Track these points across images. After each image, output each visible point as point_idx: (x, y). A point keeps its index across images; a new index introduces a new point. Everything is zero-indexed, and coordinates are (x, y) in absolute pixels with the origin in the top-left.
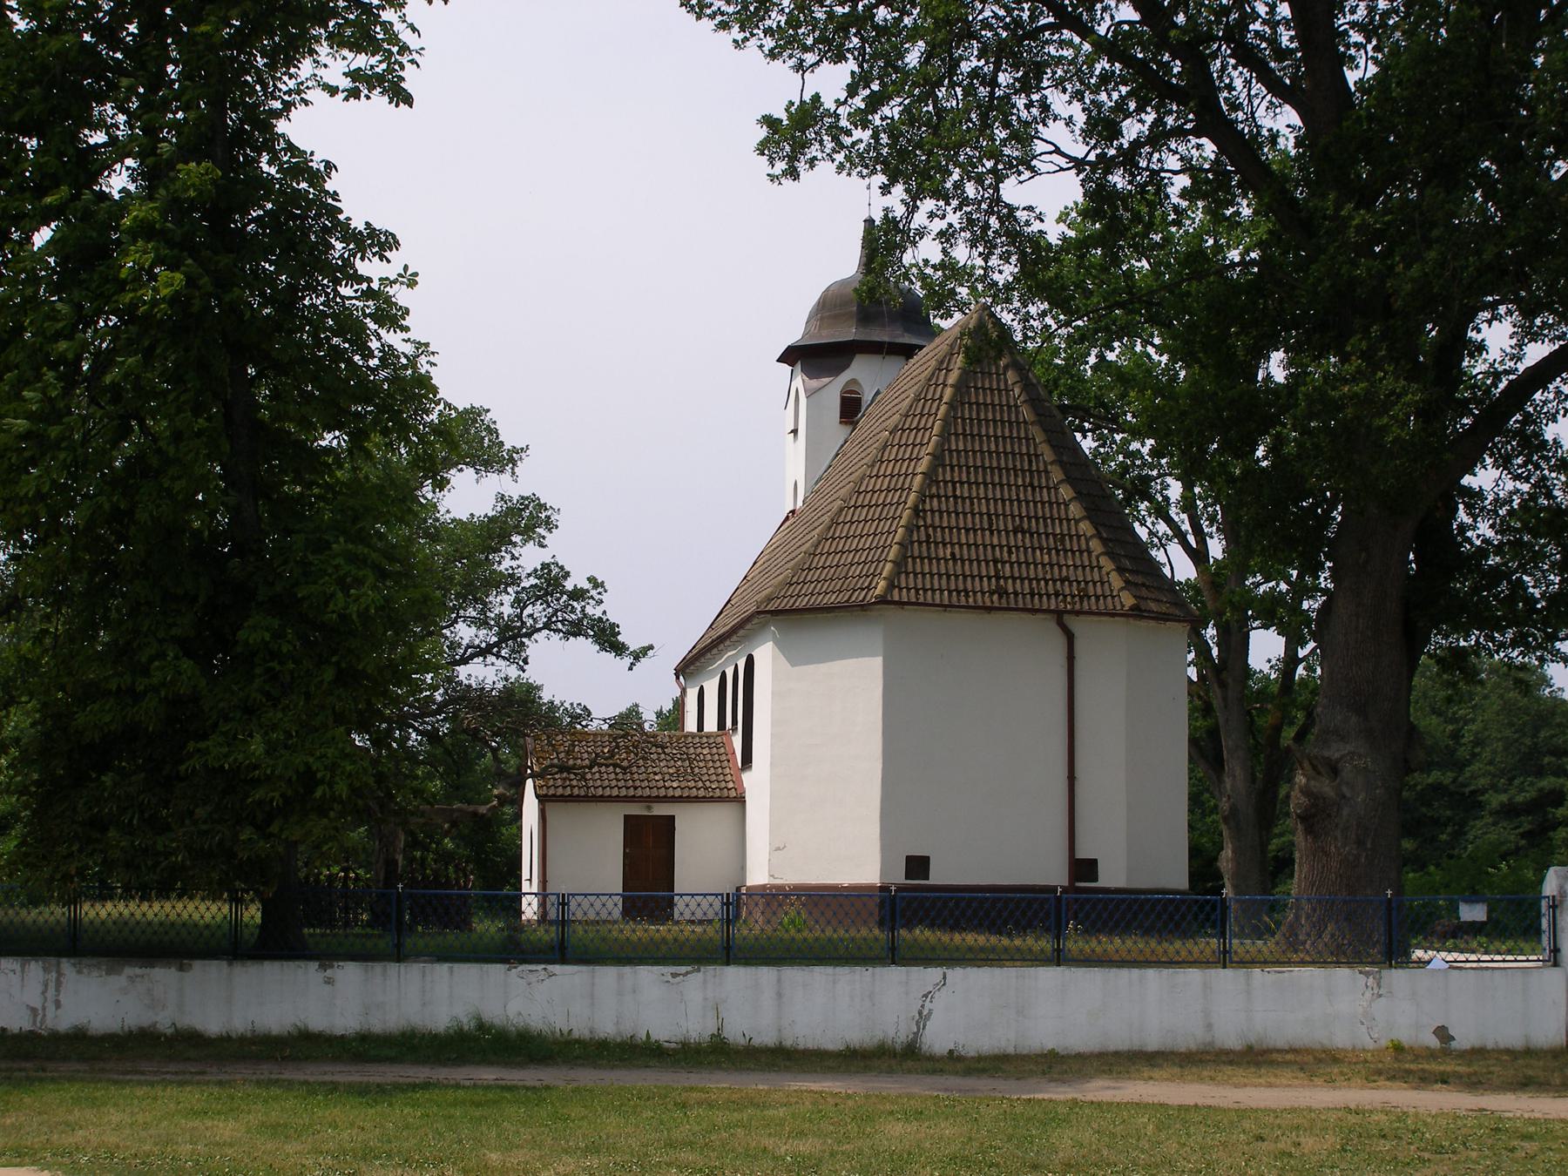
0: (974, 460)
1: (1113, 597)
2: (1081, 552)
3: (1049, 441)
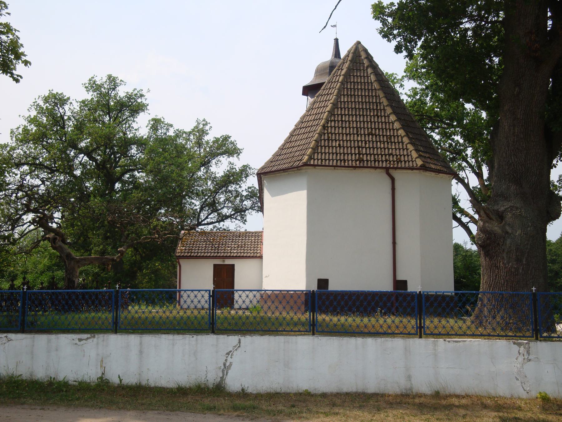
0: (352, 106)
1: (413, 162)
2: (399, 143)
3: (386, 97)
